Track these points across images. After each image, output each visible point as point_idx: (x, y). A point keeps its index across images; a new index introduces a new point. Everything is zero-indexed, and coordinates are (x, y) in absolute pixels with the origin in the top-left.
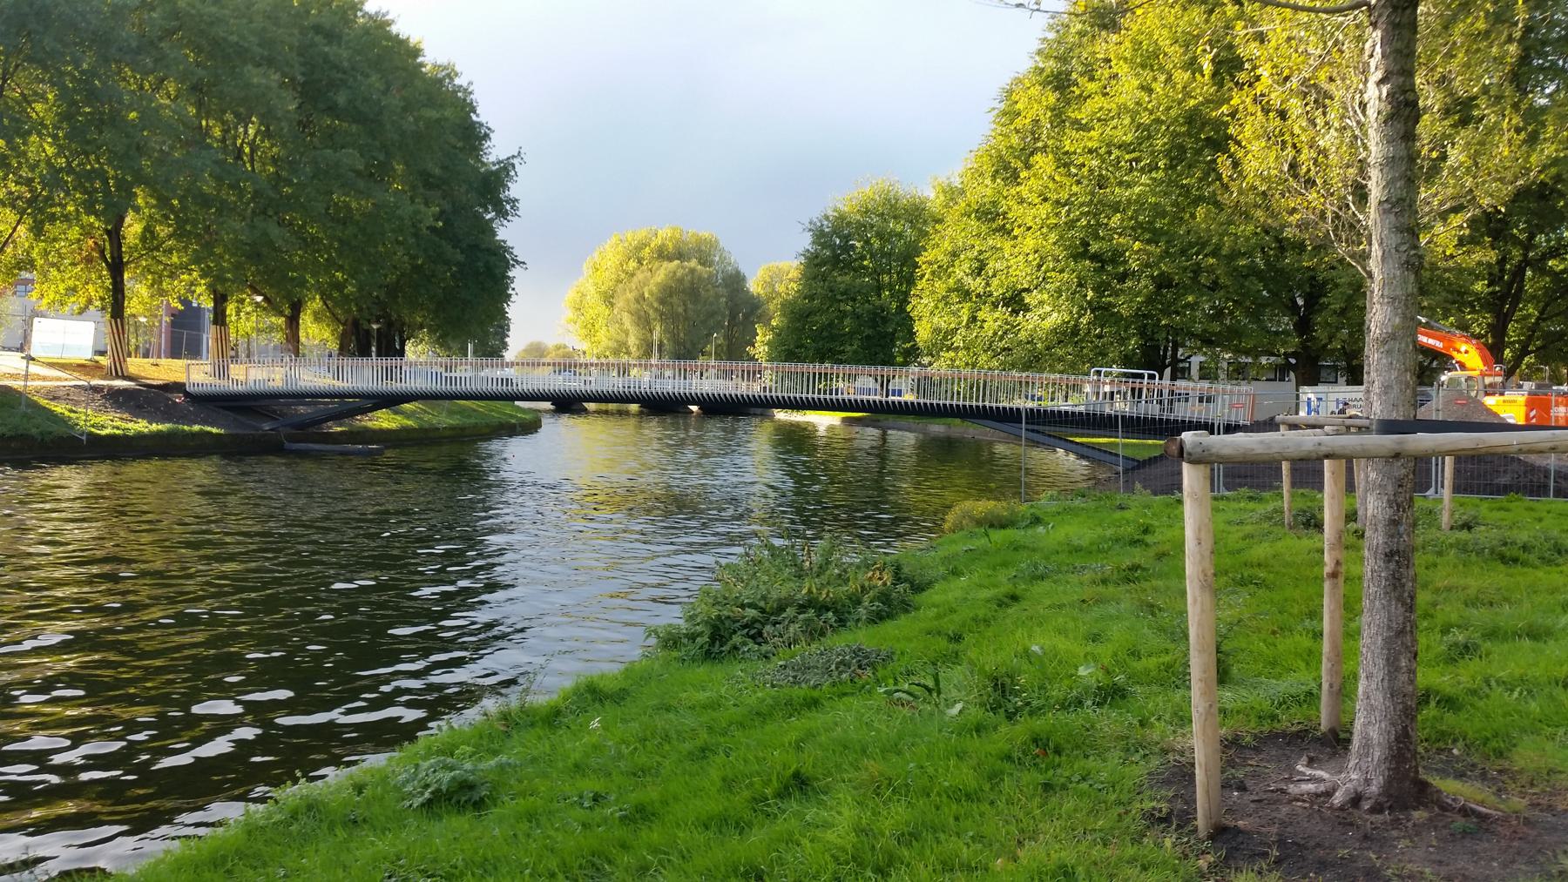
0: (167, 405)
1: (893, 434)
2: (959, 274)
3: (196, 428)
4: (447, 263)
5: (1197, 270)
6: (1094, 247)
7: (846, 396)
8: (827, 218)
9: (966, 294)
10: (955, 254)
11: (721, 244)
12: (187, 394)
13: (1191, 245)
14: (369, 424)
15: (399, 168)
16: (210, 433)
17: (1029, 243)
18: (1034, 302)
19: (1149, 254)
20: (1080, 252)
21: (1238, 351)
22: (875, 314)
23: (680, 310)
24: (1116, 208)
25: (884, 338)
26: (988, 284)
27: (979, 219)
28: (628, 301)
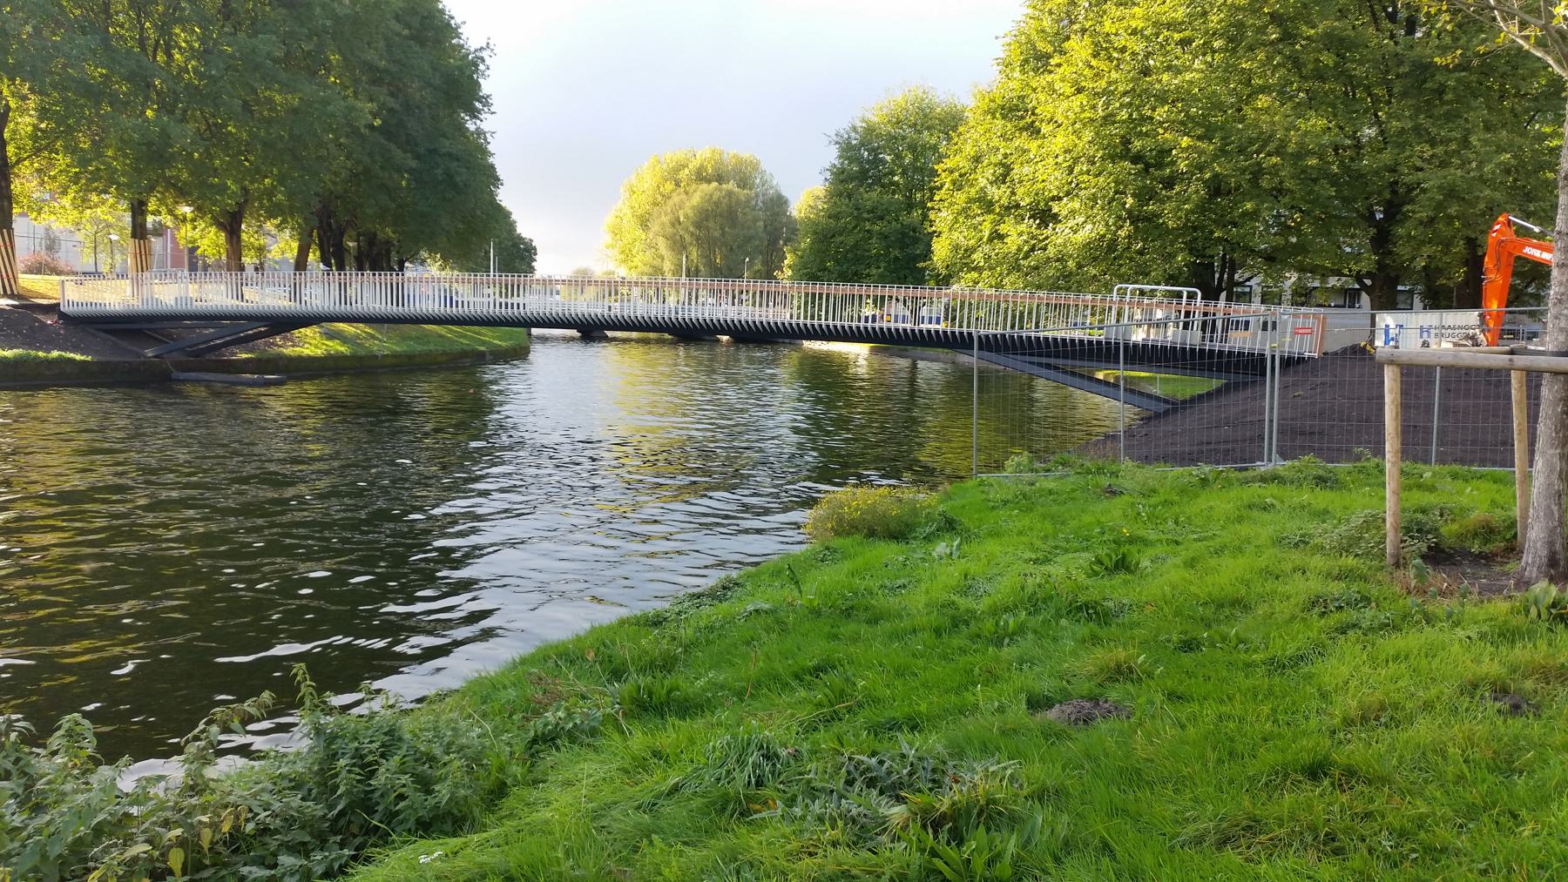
0: (32, 328)
1: (921, 364)
2: (982, 182)
3: (55, 354)
4: (399, 170)
5: (1258, 172)
6: (1137, 144)
7: (885, 325)
8: (854, 129)
9: (988, 206)
10: (977, 159)
11: (763, 166)
12: (63, 316)
13: (1251, 142)
14: (289, 351)
15: (335, 58)
16: (72, 361)
17: (1060, 141)
18: (1064, 213)
19: (1201, 153)
20: (1121, 151)
21: (1301, 269)
22: (904, 235)
23: (717, 234)
24: (1162, 99)
25: (906, 260)
26: (1013, 193)
27: (1004, 117)
28: (663, 224)
